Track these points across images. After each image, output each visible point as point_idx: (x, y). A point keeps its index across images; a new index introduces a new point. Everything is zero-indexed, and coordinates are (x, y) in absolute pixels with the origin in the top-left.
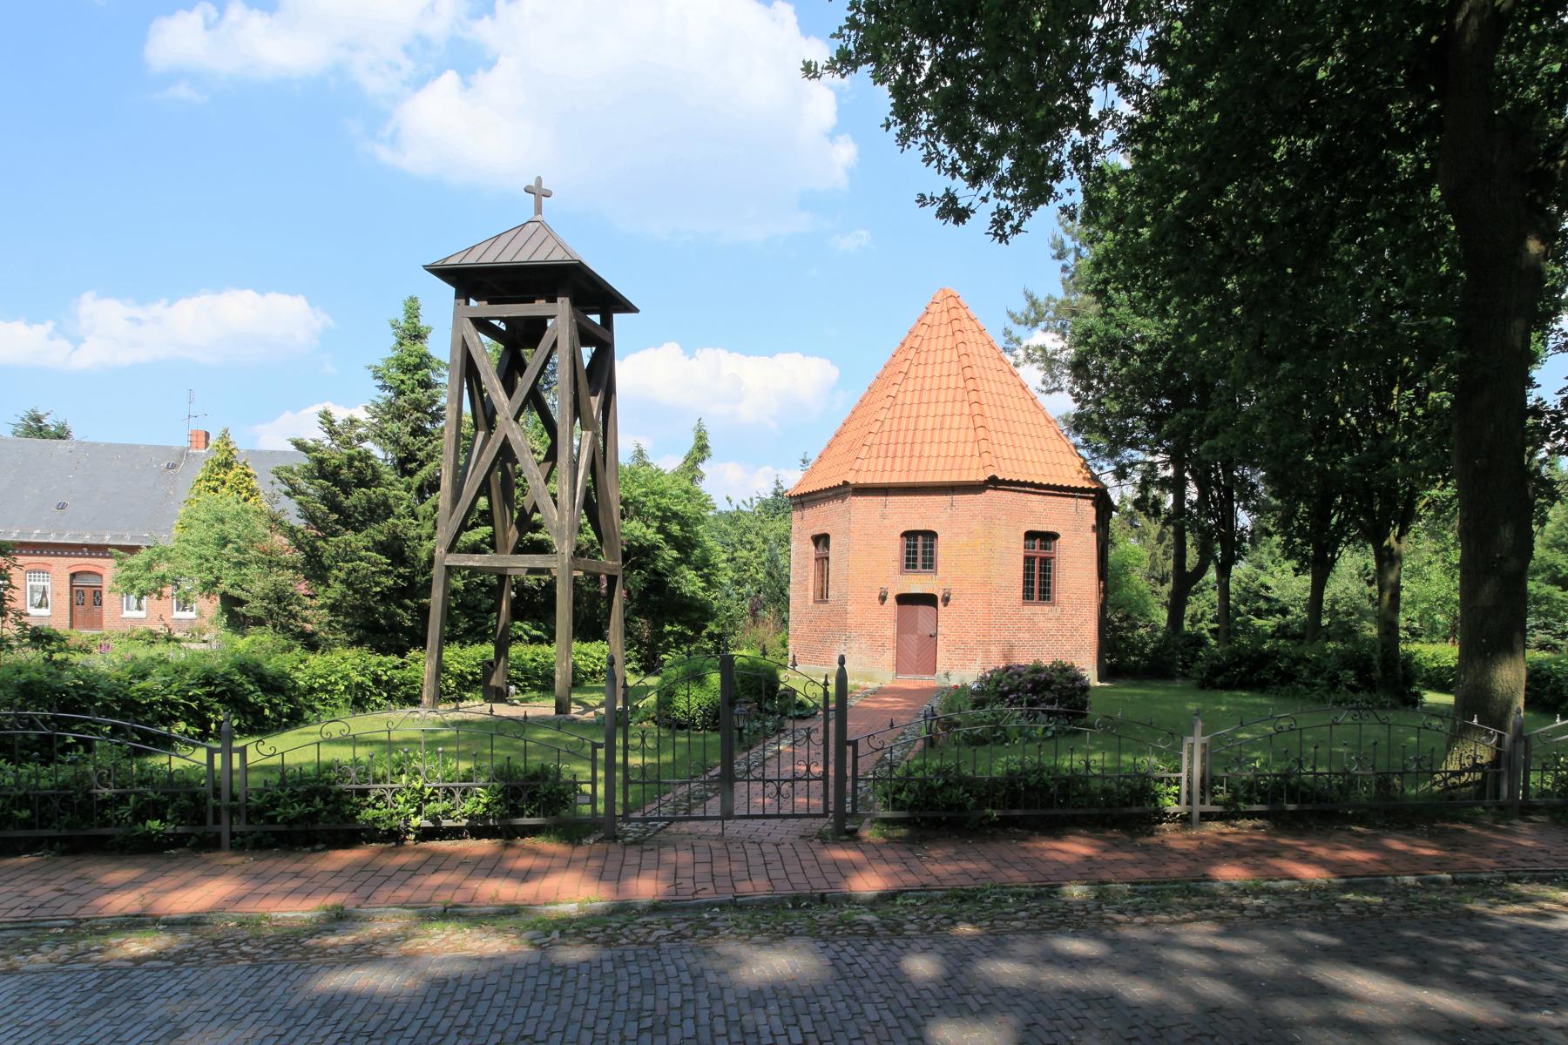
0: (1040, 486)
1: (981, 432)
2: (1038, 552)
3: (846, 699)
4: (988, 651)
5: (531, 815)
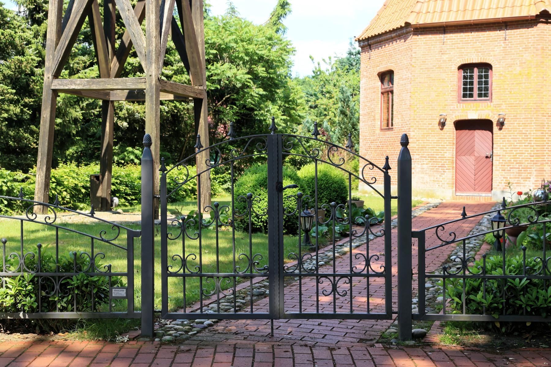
3: (410, 211)
5: (63, 309)
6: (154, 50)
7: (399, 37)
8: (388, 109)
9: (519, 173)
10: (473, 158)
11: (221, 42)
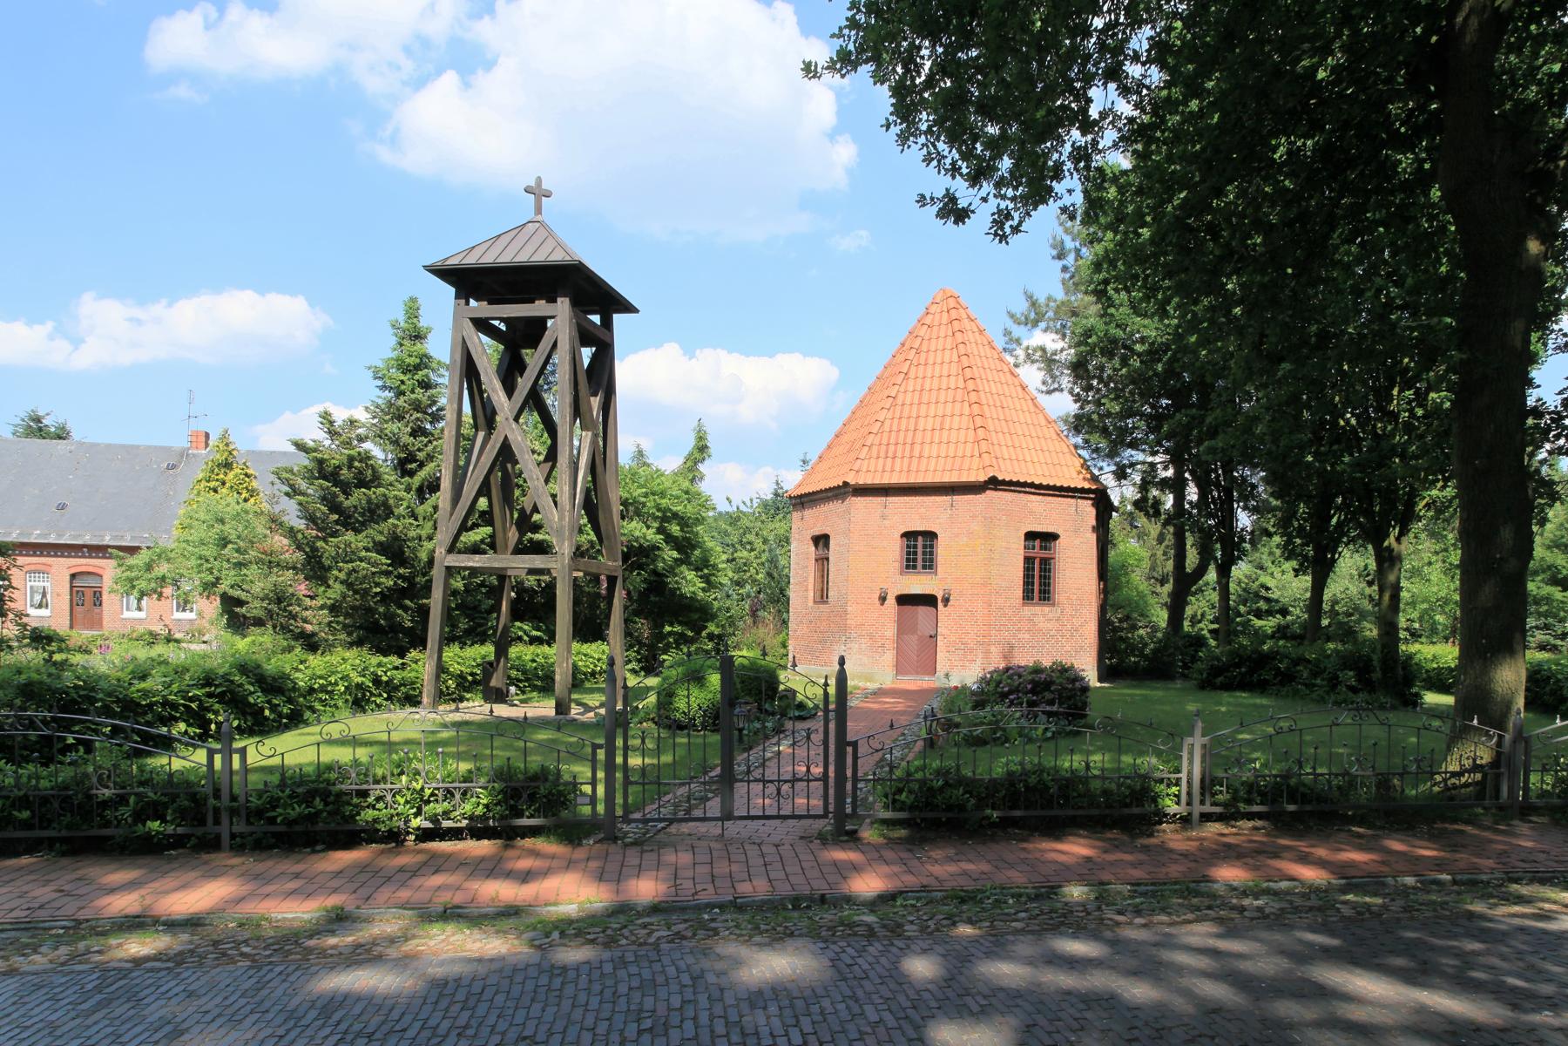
0: (1040, 486)
1: (981, 432)
2: (1038, 553)
3: (846, 699)
4: (988, 652)
5: (531, 816)
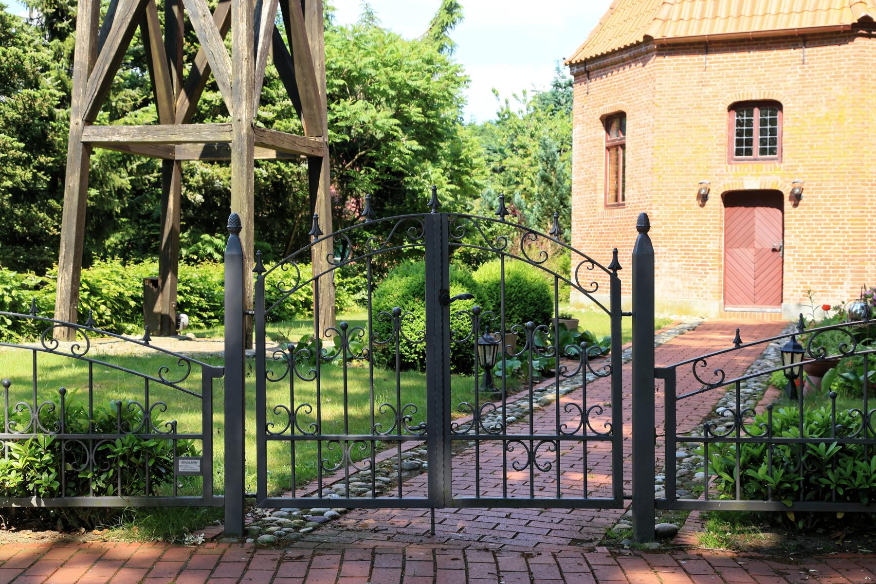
3: (652, 336)
5: (100, 492)
6: (244, 80)
7: (635, 59)
8: (617, 173)
9: (825, 275)
10: (752, 251)
11: (351, 67)
